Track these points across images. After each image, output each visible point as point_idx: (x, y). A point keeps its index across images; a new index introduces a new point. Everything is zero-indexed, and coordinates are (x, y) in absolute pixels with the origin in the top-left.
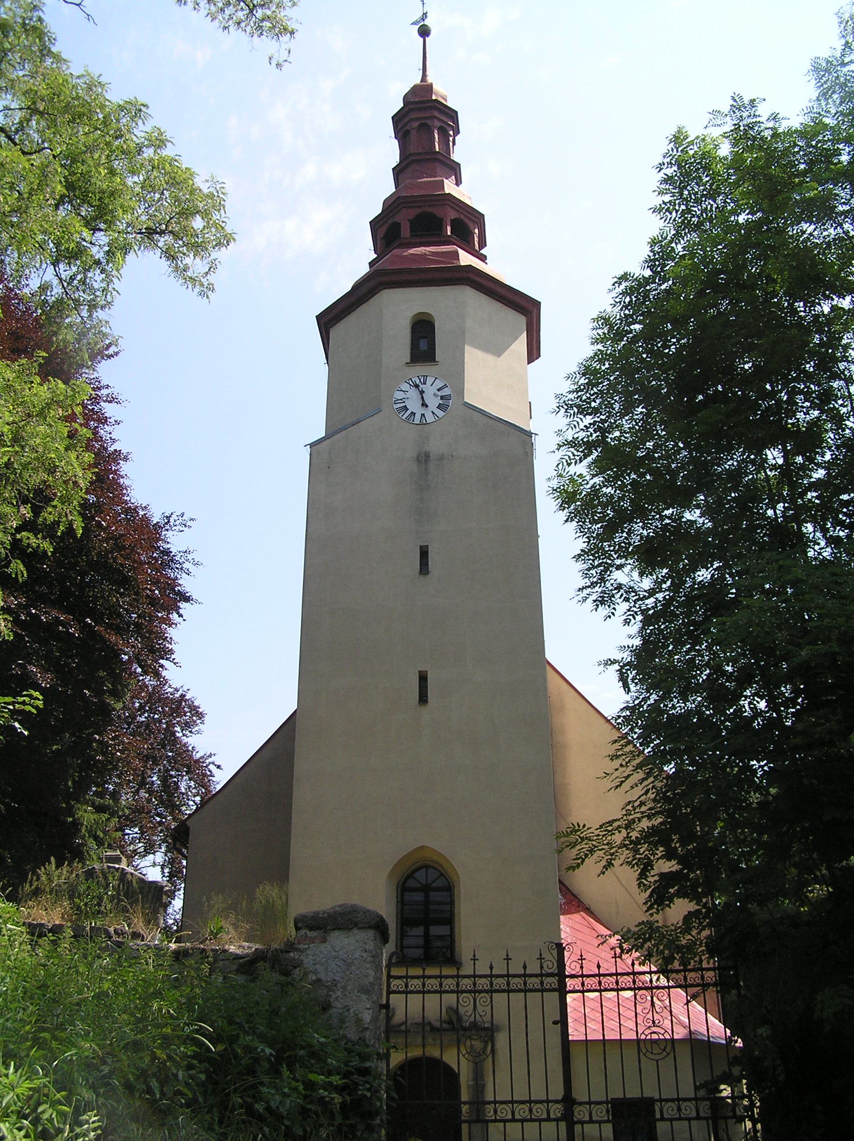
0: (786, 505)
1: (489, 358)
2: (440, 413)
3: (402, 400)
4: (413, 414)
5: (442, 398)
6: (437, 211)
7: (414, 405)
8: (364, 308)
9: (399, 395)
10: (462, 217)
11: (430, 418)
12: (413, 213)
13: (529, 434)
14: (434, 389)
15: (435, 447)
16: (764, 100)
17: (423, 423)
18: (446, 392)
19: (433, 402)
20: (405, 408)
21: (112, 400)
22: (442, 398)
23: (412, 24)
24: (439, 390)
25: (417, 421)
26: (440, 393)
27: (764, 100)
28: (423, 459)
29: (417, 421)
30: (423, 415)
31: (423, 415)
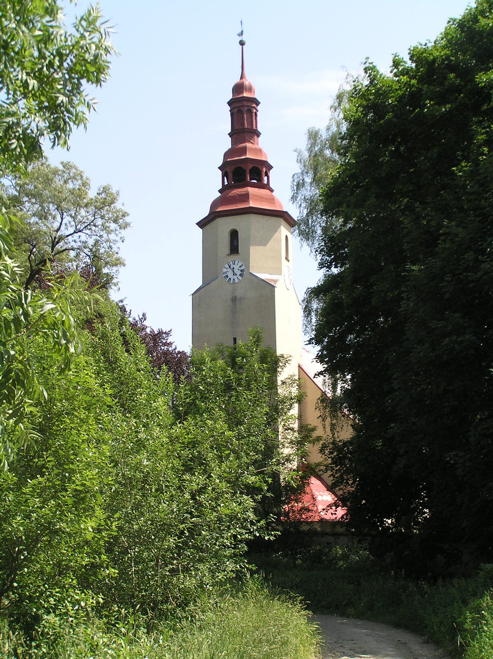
0: (462, 83)
1: (262, 248)
2: (240, 278)
3: (226, 272)
4: (230, 279)
5: (241, 271)
6: (242, 166)
7: (230, 275)
8: (212, 224)
9: (225, 270)
10: (256, 165)
11: (236, 281)
12: (233, 167)
13: (274, 287)
14: (238, 267)
15: (239, 294)
16: (123, 241)
17: (234, 283)
18: (243, 268)
19: (238, 273)
20: (227, 276)
21: (300, 154)
22: (241, 271)
23: (242, 31)
24: (240, 267)
25: (232, 282)
26: (240, 269)
27: (123, 241)
28: (234, 299)
29: (232, 282)
30: (234, 279)
31: (234, 279)
